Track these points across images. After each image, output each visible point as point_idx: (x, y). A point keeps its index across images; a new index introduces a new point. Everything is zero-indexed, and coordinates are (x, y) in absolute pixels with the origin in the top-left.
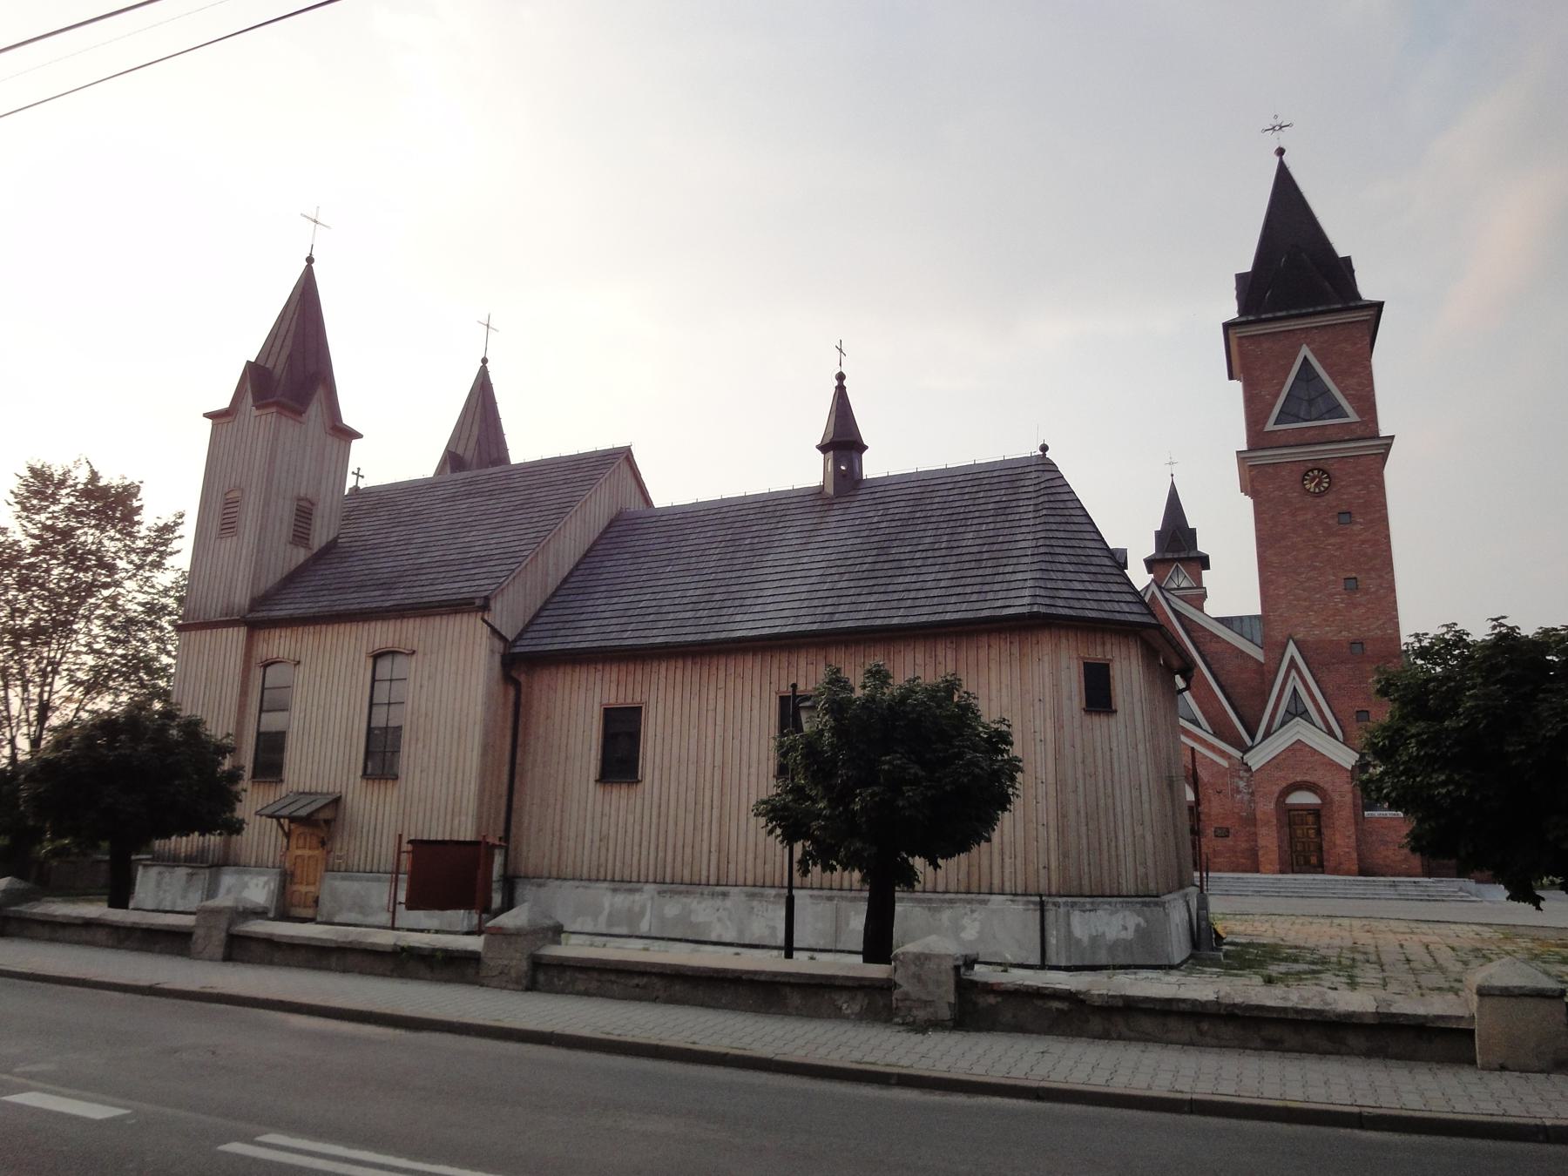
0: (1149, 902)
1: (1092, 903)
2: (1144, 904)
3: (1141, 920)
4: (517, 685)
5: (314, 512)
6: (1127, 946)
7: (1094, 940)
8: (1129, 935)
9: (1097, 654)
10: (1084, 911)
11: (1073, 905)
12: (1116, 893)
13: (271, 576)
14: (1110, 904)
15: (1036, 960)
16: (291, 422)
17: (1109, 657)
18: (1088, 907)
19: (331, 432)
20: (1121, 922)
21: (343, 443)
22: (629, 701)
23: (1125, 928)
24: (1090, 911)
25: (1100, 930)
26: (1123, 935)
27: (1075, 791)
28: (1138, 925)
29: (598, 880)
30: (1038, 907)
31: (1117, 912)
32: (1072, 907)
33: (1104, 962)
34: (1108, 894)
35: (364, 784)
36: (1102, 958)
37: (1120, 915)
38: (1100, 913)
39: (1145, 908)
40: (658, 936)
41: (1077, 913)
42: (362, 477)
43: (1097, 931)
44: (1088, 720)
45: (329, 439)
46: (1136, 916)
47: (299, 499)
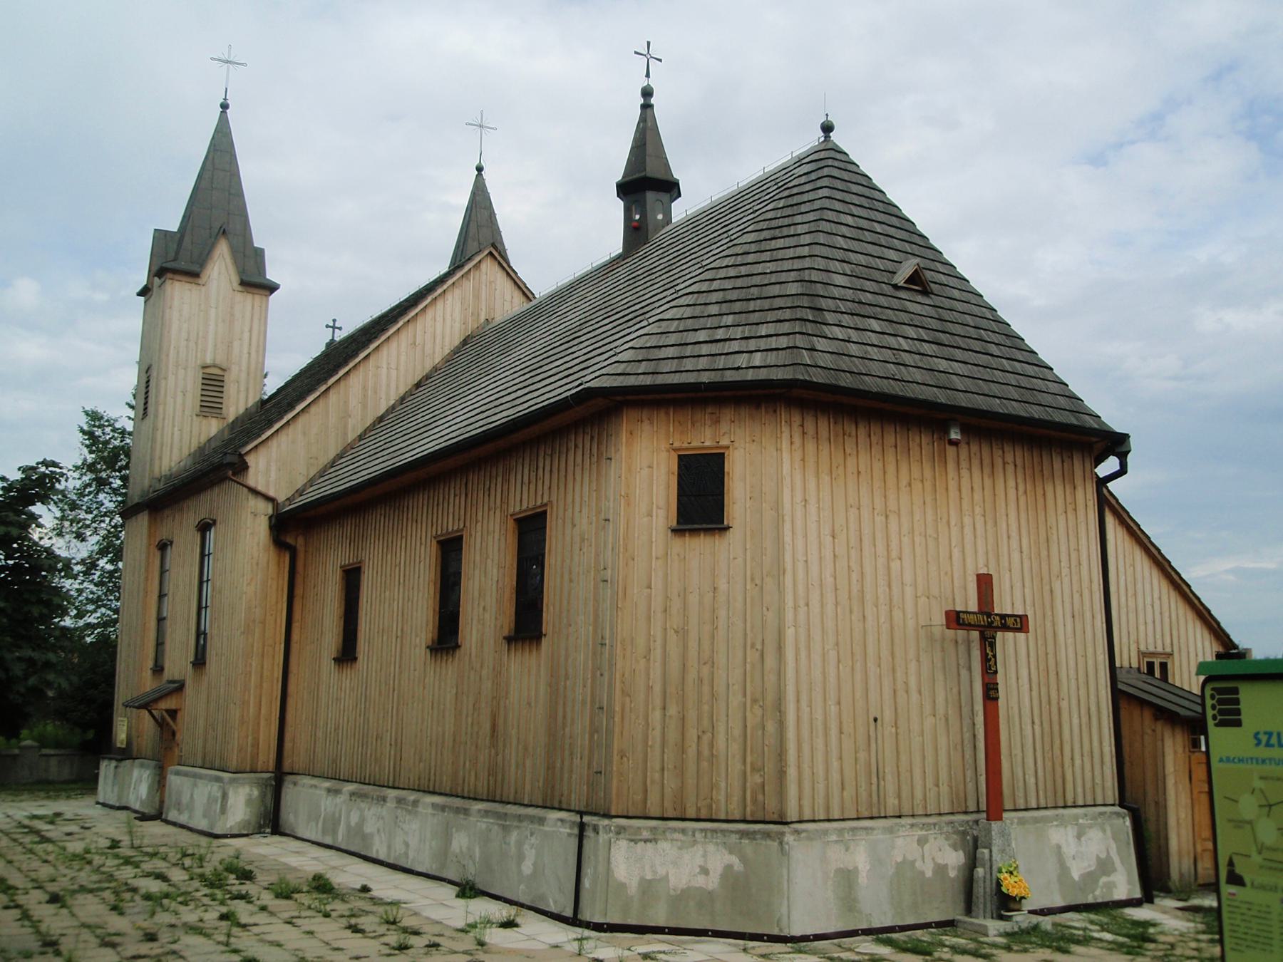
0: (755, 832)
1: (653, 829)
2: (743, 834)
3: (734, 860)
4: (293, 552)
5: (226, 379)
6: (705, 899)
7: (647, 887)
8: (712, 882)
9: (702, 438)
10: (636, 842)
11: (620, 831)
12: (703, 814)
13: (176, 451)
14: (683, 831)
15: (569, 913)
16: (188, 286)
17: (724, 442)
18: (646, 834)
19: (240, 288)
20: (699, 861)
21: (264, 298)
22: (351, 561)
23: (705, 871)
24: (646, 841)
25: (661, 871)
26: (700, 881)
27: (647, 657)
28: (729, 867)
29: (352, 782)
30: (576, 831)
31: (695, 842)
32: (618, 833)
33: (661, 921)
34: (723, 817)
35: (337, 667)
36: (659, 918)
37: (699, 850)
38: (664, 845)
39: (746, 841)
40: (343, 847)
41: (623, 844)
42: (327, 326)
43: (655, 872)
44: (678, 544)
45: (240, 297)
46: (726, 852)
47: (204, 367)
